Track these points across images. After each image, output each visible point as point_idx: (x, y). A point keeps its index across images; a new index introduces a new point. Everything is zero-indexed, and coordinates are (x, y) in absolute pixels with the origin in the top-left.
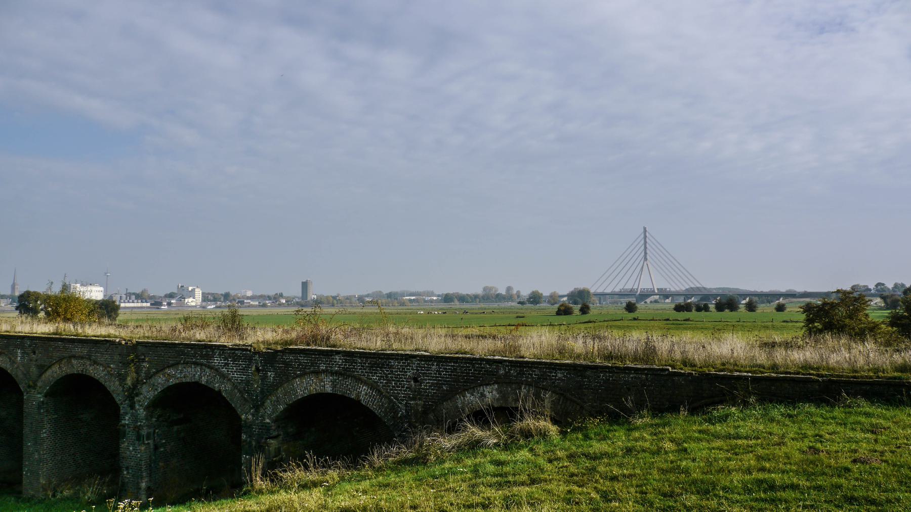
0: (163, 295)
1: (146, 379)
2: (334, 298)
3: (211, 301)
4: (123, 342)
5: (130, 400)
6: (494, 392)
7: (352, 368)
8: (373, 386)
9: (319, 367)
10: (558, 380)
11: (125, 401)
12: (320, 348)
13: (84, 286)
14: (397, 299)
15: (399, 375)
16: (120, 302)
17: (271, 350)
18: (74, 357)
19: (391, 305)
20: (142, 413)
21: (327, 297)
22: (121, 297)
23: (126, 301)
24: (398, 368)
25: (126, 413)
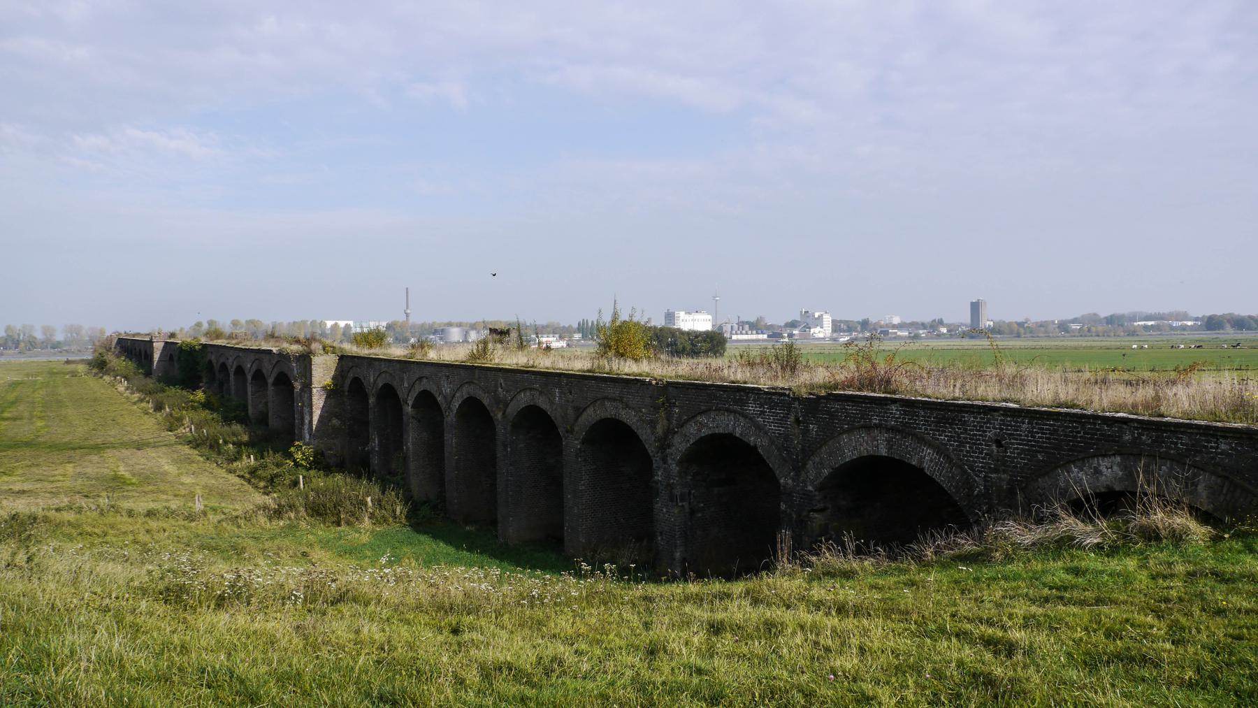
0: (783, 324)
1: (677, 428)
2: (1020, 325)
3: (844, 331)
4: (654, 382)
5: (662, 453)
6: (1115, 468)
7: (912, 423)
8: (940, 450)
9: (871, 420)
10: (1221, 454)
11: (657, 453)
12: (872, 394)
13: (690, 313)
14: (1122, 325)
15: (976, 435)
16: (731, 334)
17: (813, 395)
18: (607, 398)
19: (1113, 334)
20: (675, 468)
21: (1010, 324)
22: (732, 326)
23: (739, 332)
24: (974, 426)
25: (659, 468)
